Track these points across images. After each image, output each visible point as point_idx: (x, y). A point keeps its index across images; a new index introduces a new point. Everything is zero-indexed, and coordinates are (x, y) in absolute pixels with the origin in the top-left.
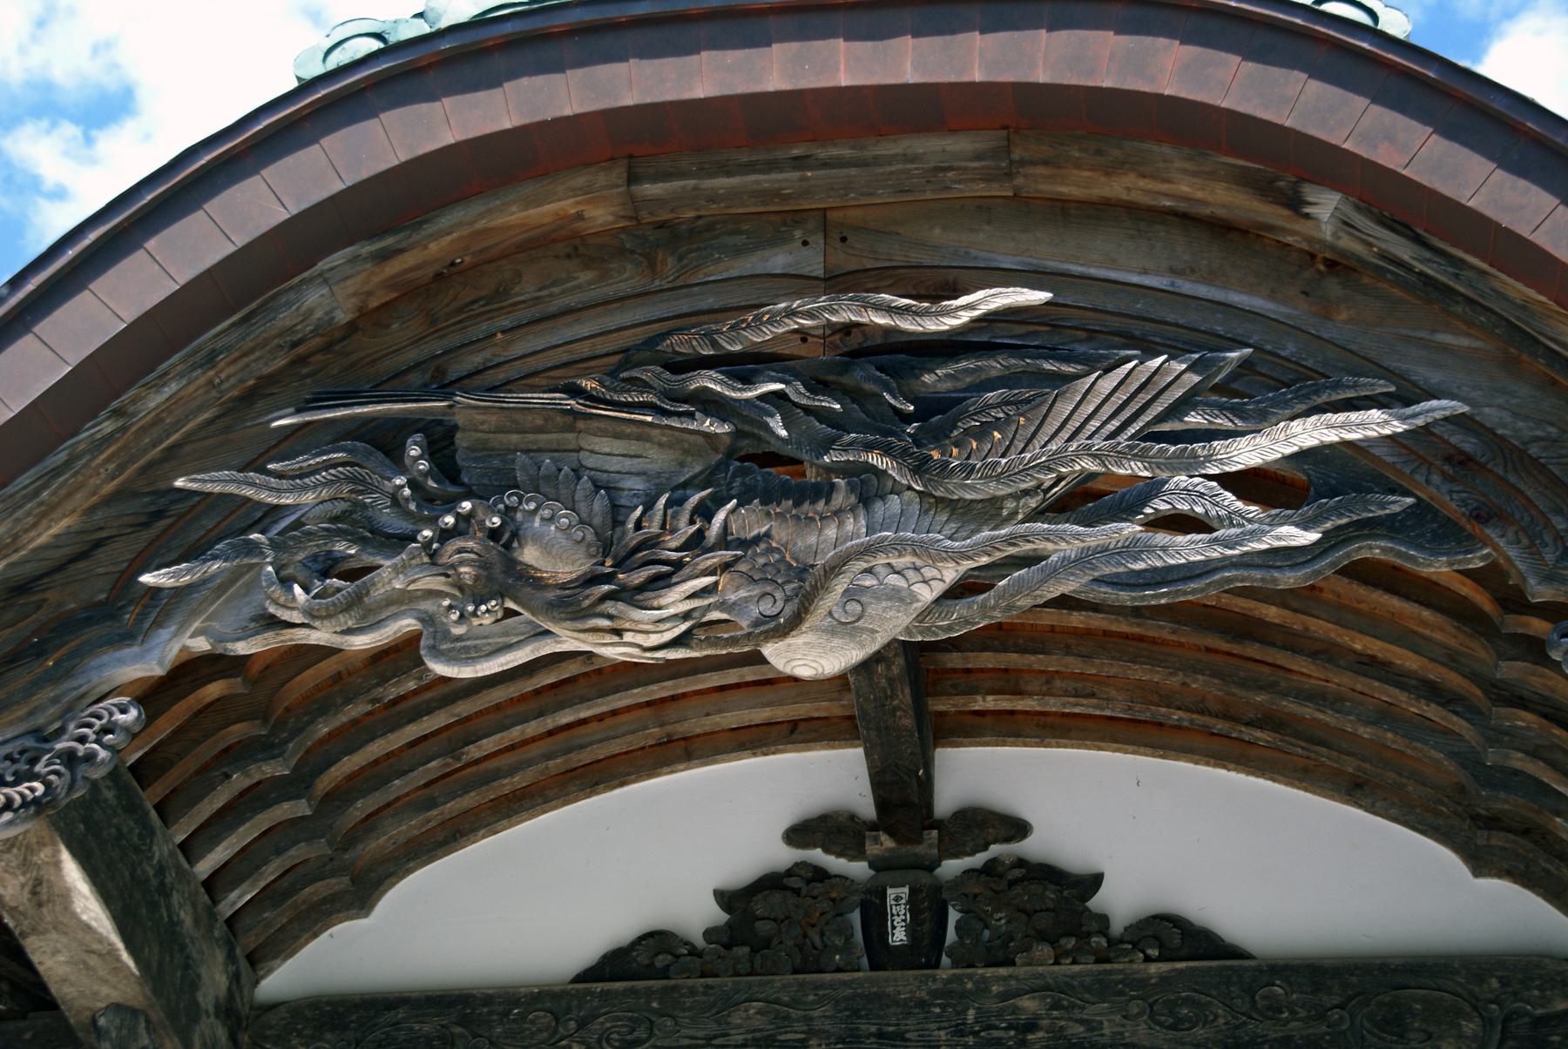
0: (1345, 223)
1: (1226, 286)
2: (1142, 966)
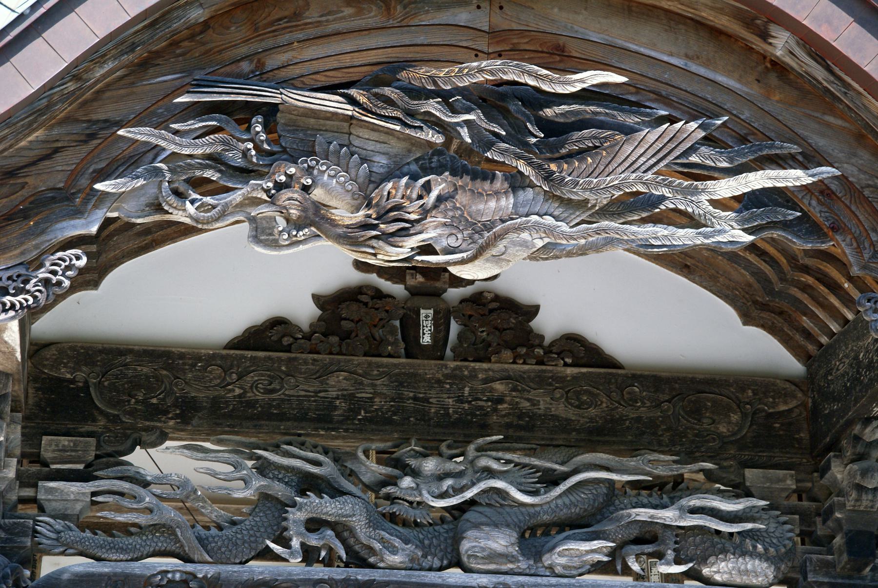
0: (791, 52)
1: (715, 70)
2: (563, 369)
